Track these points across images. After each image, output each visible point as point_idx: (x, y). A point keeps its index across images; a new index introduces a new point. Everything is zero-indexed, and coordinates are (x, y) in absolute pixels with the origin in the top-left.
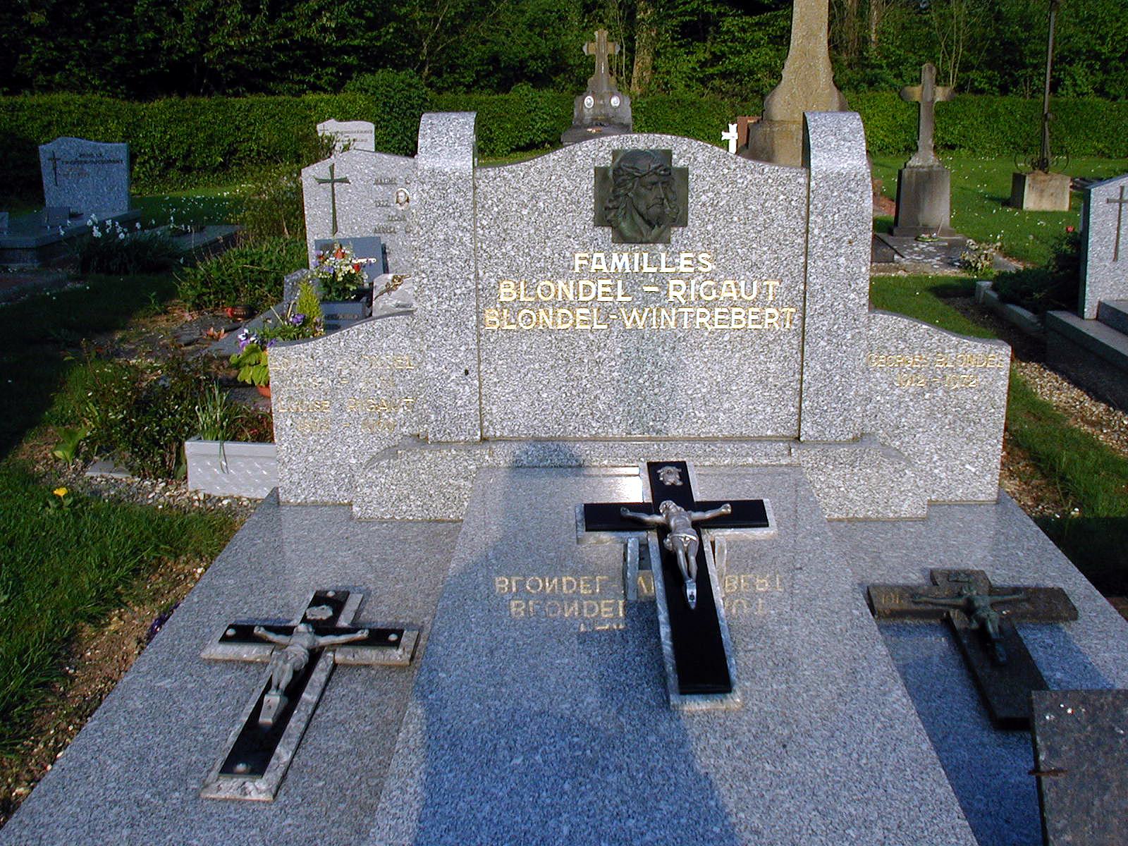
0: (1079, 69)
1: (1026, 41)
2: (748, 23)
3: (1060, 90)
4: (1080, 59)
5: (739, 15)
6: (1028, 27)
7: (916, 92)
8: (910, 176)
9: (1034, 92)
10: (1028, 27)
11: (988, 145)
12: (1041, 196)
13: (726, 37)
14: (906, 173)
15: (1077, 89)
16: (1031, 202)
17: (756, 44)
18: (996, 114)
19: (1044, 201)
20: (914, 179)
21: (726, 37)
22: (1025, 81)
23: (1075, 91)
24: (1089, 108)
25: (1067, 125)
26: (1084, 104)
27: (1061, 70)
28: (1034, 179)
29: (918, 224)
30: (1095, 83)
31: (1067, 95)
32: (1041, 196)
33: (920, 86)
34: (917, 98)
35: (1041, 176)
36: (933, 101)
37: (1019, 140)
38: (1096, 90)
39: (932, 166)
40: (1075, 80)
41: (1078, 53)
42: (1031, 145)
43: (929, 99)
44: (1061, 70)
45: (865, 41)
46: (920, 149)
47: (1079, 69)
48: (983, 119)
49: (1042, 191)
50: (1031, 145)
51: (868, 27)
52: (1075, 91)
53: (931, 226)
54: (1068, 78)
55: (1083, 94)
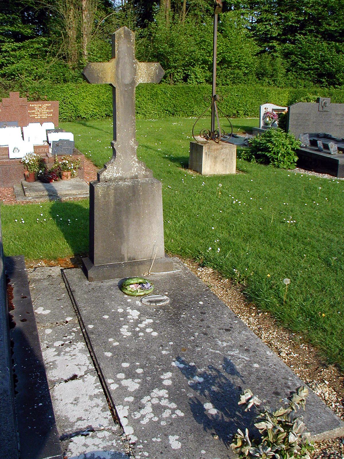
0: (197, 69)
1: (172, 53)
2: (17, 46)
3: (189, 81)
4: (198, 64)
5: (12, 42)
6: (172, 45)
7: (107, 71)
8: (106, 195)
9: (175, 82)
10: (172, 45)
11: (152, 112)
12: (215, 162)
13: (5, 54)
14: (99, 189)
15: (198, 80)
16: (209, 167)
17: (22, 57)
18: (156, 94)
19: (218, 165)
20: (112, 198)
21: (5, 54)
22: (170, 76)
23: (197, 81)
24: (206, 90)
25: (195, 100)
26: (203, 88)
27: (189, 70)
28: (209, 148)
29: (122, 259)
30: (206, 77)
31: (192, 83)
32: (215, 162)
33: (113, 62)
34: (109, 80)
35: (215, 146)
36: (133, 82)
37: (169, 109)
38: (207, 81)
39: (136, 177)
40: (196, 75)
41: (198, 60)
42: (176, 111)
43: (127, 81)
44: (189, 70)
45: (81, 54)
46: (118, 153)
47: (197, 69)
48: (150, 97)
49: (216, 158)
50: (176, 111)
51: (82, 47)
52: (197, 81)
53: (141, 257)
54: (193, 74)
55: (200, 83)
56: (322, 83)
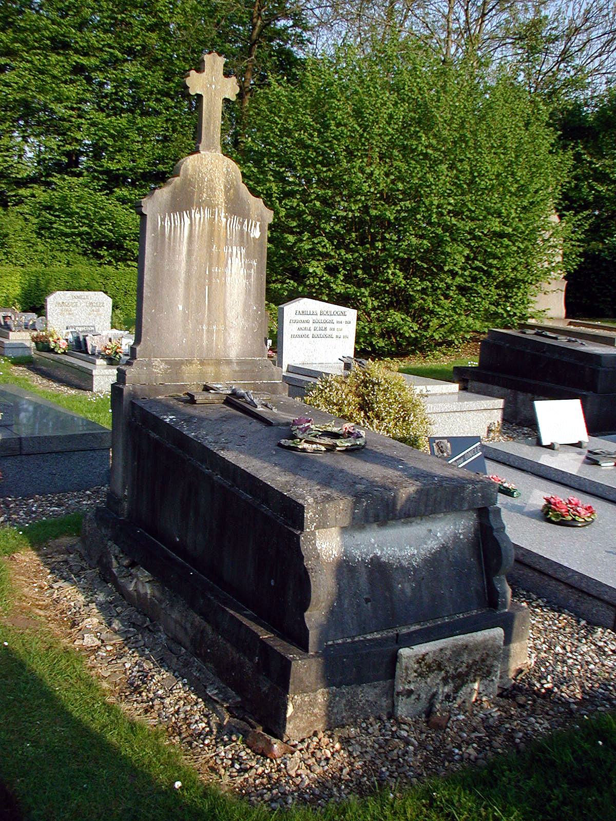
56: (100, 257)
